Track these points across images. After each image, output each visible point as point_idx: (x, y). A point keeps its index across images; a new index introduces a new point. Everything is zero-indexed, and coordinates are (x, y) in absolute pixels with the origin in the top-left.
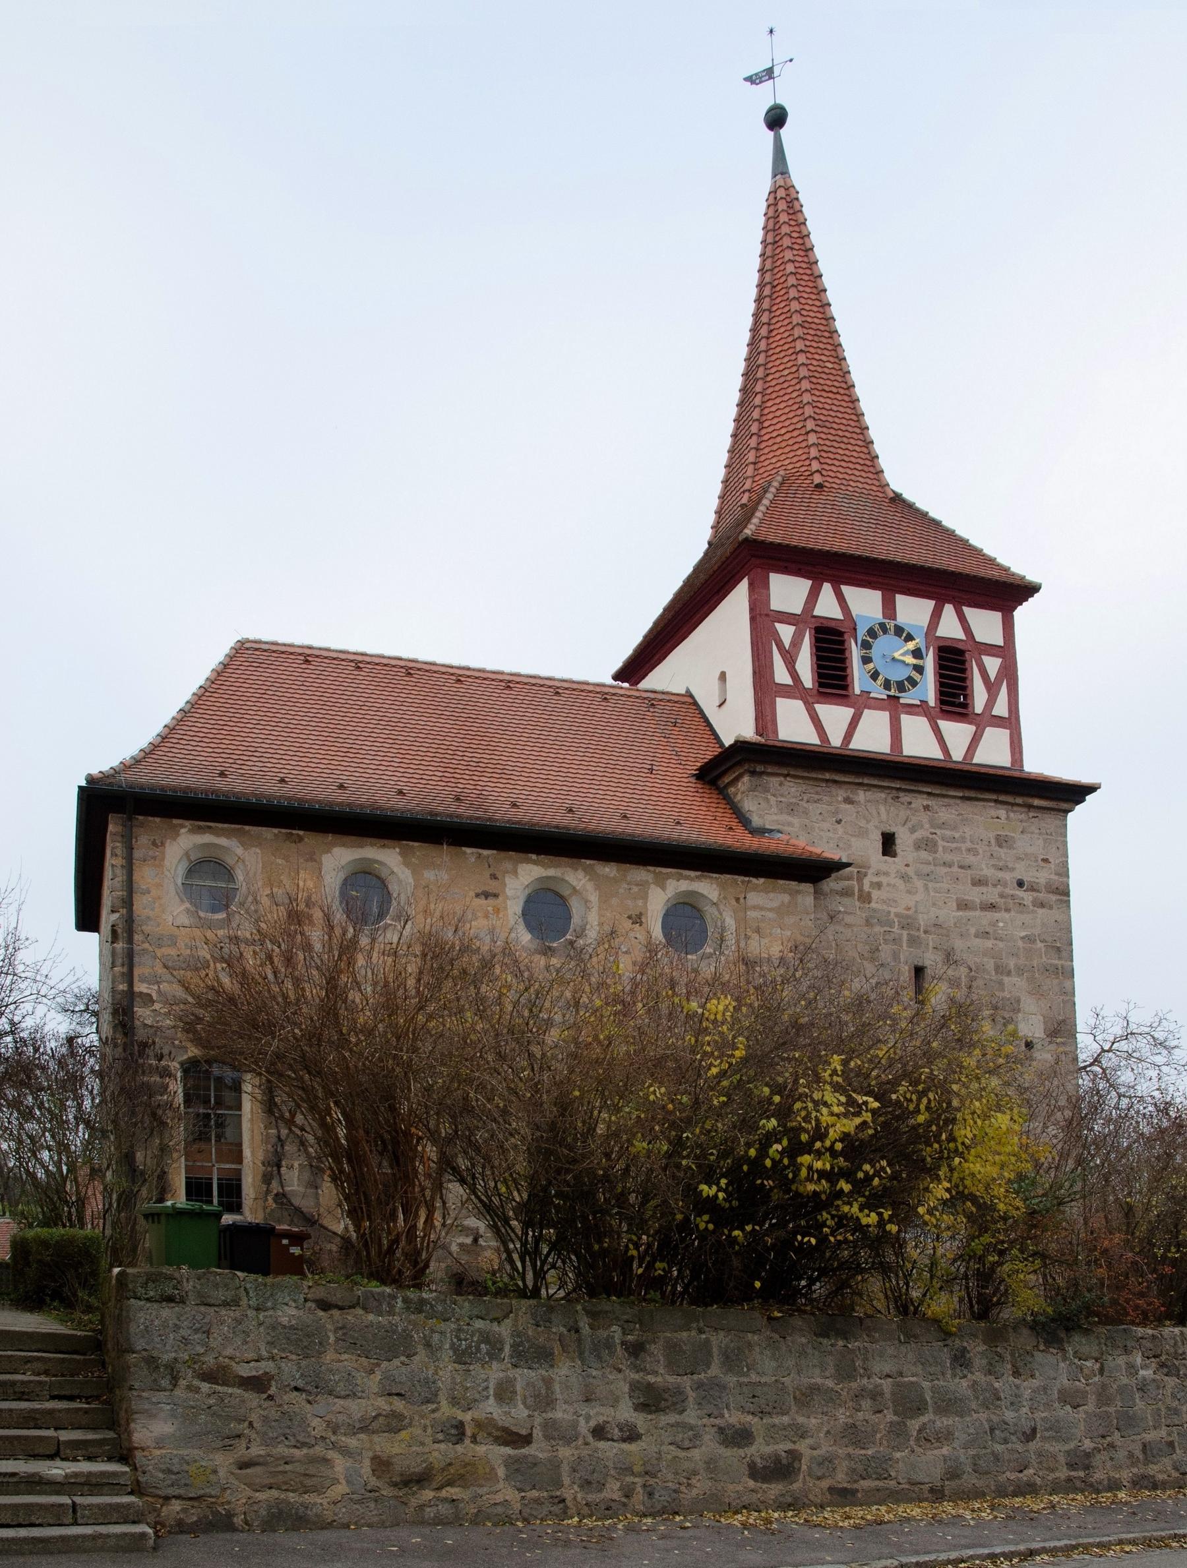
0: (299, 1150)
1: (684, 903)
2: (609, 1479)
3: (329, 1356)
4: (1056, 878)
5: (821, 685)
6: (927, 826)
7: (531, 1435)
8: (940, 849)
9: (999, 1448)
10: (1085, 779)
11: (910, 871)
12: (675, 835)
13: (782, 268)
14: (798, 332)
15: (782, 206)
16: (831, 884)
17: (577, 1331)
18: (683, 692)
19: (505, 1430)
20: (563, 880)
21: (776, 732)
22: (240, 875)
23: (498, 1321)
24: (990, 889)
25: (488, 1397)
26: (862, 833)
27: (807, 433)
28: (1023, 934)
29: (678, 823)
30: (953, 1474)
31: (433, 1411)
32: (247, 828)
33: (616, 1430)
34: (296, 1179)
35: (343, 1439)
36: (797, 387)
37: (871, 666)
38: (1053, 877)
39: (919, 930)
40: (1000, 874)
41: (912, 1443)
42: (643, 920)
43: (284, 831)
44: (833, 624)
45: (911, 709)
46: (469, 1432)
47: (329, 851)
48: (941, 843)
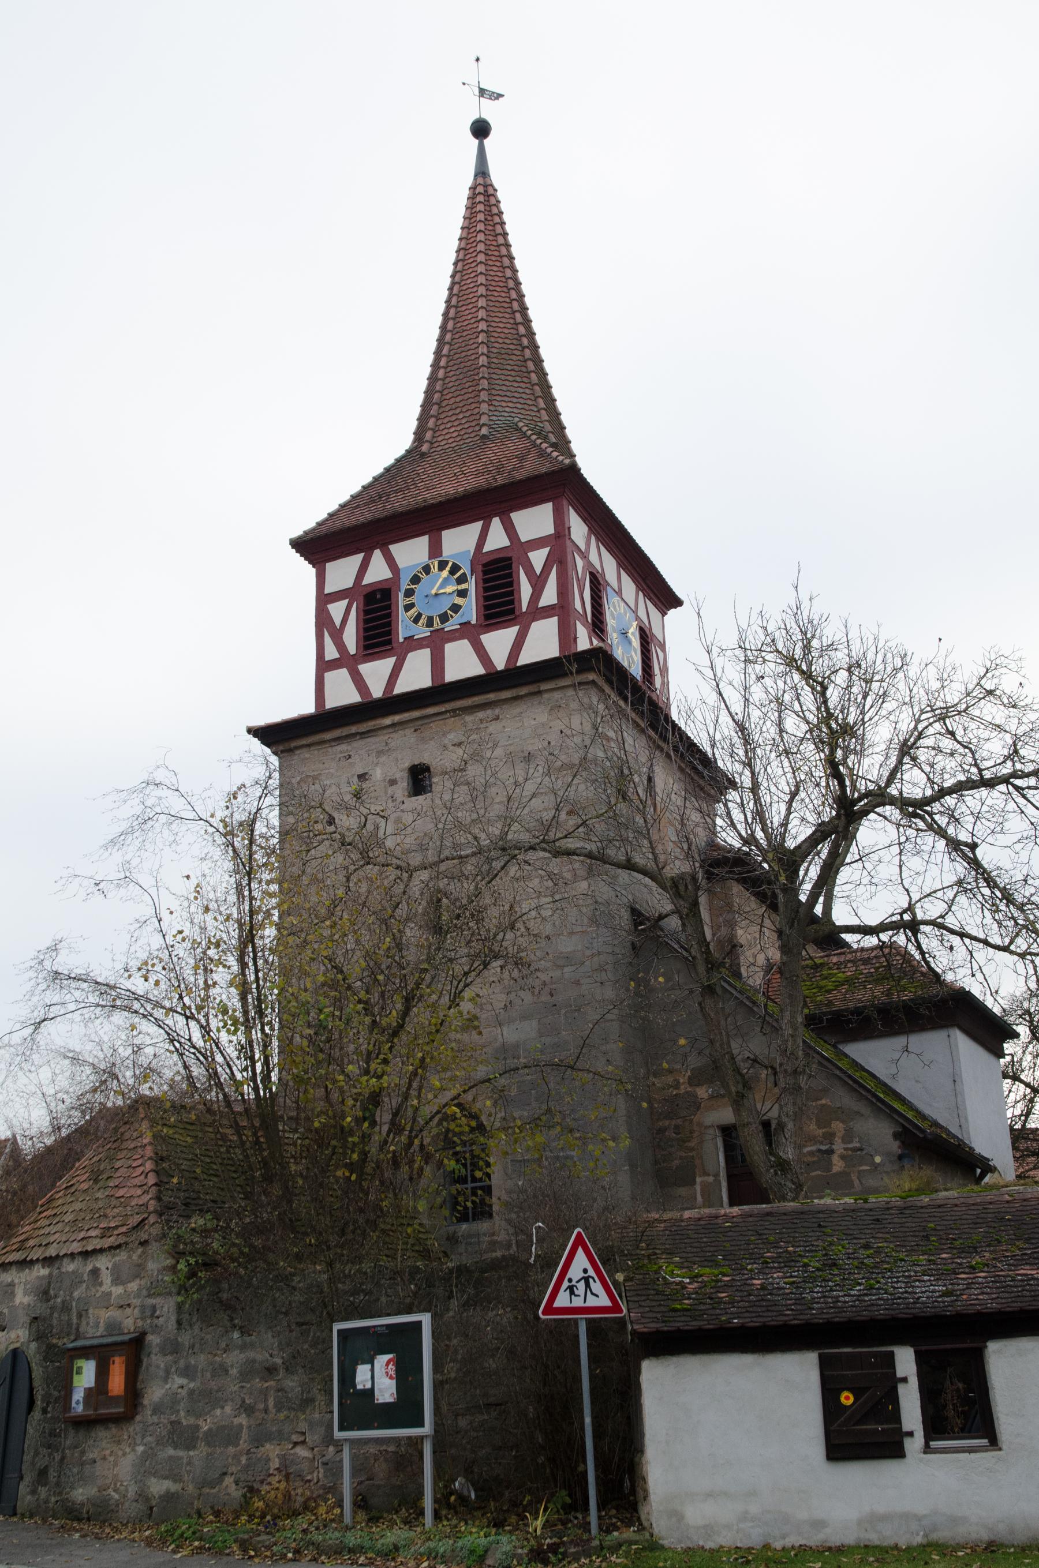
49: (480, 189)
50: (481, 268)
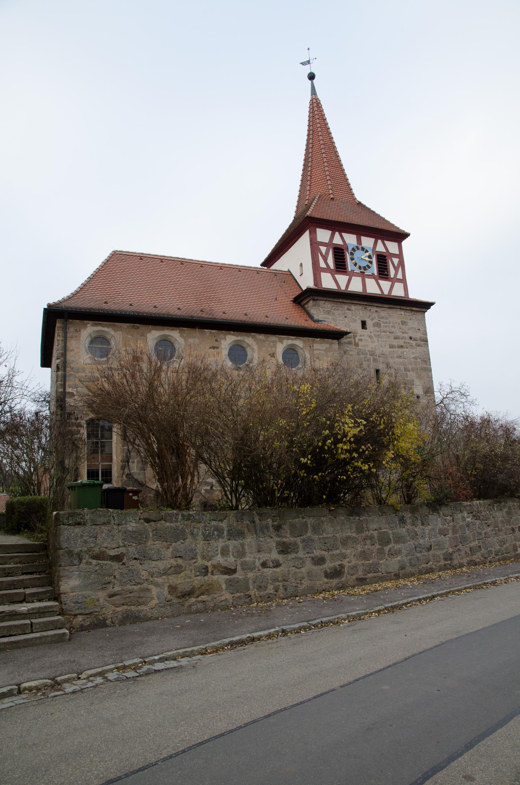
0: (137, 455)
1: (290, 349)
2: (269, 585)
3: (150, 543)
4: (423, 335)
5: (337, 268)
6: (377, 318)
7: (236, 569)
8: (382, 326)
9: (419, 555)
10: (430, 300)
11: (372, 334)
12: (286, 323)
13: (316, 125)
14: (322, 146)
15: (315, 105)
16: (344, 340)
17: (254, 522)
18: (287, 270)
19: (225, 568)
20: (244, 341)
21: (321, 285)
22: (113, 343)
23: (221, 521)
24: (400, 340)
25: (218, 554)
26: (354, 321)
27: (327, 180)
28: (413, 356)
29: (267, 317)
30: (402, 568)
31: (195, 563)
32: (116, 324)
33: (271, 563)
34: (135, 467)
35: (156, 579)
36: (323, 165)
37: (354, 261)
38: (422, 335)
39: (376, 356)
40: (404, 335)
41: (386, 556)
42: (275, 355)
43: (131, 324)
44: (340, 247)
45: (369, 276)
46: (210, 570)
47: (150, 332)
48: (382, 324)
49: (314, 101)
50: (319, 129)
